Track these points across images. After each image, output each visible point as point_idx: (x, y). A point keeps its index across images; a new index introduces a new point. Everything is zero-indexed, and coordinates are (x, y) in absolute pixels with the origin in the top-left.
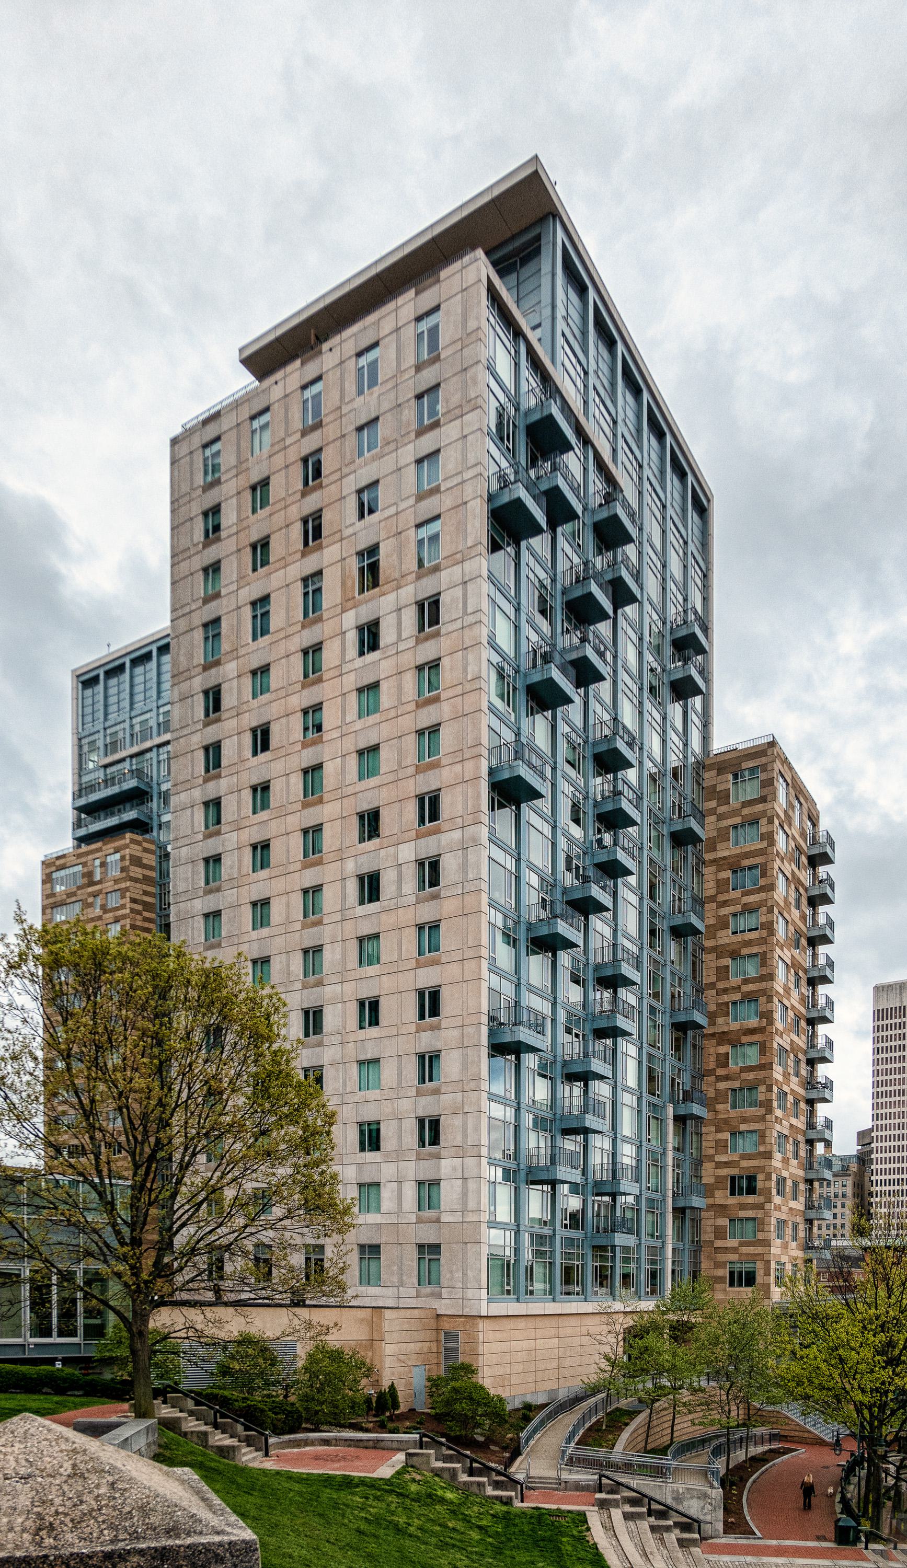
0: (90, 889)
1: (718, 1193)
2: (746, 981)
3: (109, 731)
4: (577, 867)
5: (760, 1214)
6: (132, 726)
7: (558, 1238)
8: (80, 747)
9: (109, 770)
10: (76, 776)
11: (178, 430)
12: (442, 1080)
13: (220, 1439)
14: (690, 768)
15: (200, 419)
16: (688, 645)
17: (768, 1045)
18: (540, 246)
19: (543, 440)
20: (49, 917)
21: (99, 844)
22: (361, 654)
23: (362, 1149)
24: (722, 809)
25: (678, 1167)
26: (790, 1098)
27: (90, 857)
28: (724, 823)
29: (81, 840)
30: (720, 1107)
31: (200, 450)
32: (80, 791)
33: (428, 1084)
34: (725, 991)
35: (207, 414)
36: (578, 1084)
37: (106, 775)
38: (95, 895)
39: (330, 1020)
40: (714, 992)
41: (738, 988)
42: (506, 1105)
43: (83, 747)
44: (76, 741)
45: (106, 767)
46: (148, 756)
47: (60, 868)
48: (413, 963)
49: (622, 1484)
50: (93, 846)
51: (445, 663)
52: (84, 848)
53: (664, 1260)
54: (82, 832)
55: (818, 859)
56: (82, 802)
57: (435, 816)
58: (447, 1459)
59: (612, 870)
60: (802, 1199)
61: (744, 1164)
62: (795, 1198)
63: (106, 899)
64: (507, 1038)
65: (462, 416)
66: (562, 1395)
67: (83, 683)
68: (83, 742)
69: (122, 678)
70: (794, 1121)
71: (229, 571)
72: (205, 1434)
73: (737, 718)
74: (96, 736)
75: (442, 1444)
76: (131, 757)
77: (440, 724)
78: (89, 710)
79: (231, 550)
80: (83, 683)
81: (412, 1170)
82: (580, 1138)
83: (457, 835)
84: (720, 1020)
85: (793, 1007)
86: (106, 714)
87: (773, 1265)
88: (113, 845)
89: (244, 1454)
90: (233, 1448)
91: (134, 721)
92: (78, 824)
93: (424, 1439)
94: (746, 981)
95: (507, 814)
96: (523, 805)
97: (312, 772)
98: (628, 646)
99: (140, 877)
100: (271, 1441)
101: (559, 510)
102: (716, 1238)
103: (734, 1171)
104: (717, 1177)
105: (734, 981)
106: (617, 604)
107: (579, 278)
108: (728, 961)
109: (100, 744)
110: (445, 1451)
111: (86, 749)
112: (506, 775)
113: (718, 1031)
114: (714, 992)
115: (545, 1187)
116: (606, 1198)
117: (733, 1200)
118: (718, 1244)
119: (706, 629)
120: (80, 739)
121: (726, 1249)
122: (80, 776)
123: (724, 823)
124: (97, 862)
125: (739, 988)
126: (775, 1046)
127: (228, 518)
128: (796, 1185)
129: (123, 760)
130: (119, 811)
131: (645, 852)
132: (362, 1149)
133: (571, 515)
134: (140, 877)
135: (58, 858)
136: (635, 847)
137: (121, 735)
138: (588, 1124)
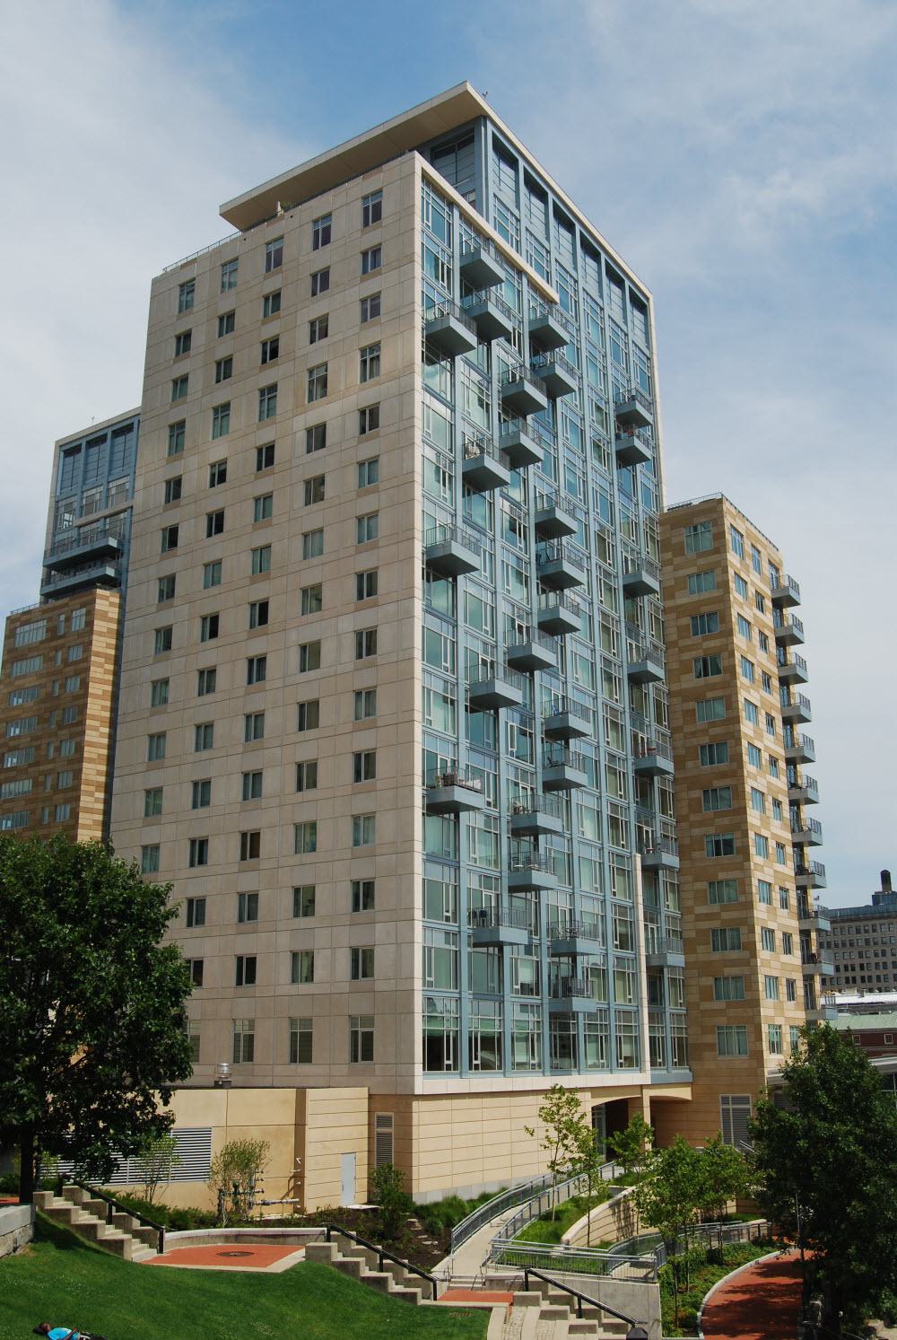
0: (53, 644)
1: (701, 949)
2: (713, 724)
3: (85, 495)
4: (520, 627)
5: (746, 971)
6: (108, 490)
7: (612, 1011)
8: (57, 509)
9: (82, 530)
10: (51, 536)
11: (159, 272)
12: (377, 842)
13: (110, 1232)
14: (642, 527)
15: (179, 264)
16: (629, 420)
17: (740, 789)
18: (473, 137)
19: (475, 278)
20: (8, 671)
21: (65, 600)
22: (309, 451)
23: (296, 915)
24: (677, 560)
25: (652, 921)
26: (772, 843)
27: (56, 612)
28: (681, 573)
29: (47, 596)
30: (696, 854)
31: (177, 290)
32: (53, 549)
33: (363, 847)
34: (693, 734)
35: (185, 261)
36: (527, 838)
37: (79, 534)
38: (56, 649)
39: (269, 783)
40: (682, 735)
41: (704, 732)
42: (444, 864)
43: (59, 507)
44: (53, 503)
45: (80, 527)
46: (122, 516)
47: (23, 624)
48: (349, 727)
49: (550, 1281)
50: (61, 602)
51: (383, 460)
52: (52, 603)
53: (639, 1027)
54: (51, 588)
55: (783, 601)
56: (54, 560)
57: (372, 591)
58: (408, 1282)
59: (554, 627)
60: (797, 953)
61: (725, 915)
62: (788, 951)
63: (68, 653)
64: (443, 798)
65: (400, 267)
66: (512, 1187)
67: (65, 451)
68: (60, 504)
69: (102, 446)
70: (779, 867)
71: (194, 386)
72: (94, 1227)
73: (681, 481)
74: (73, 499)
75: (351, 1237)
76: (105, 518)
77: (378, 511)
78: (68, 476)
79: (198, 367)
80: (65, 451)
81: (349, 937)
82: (531, 895)
83: (392, 608)
84: (690, 764)
85: (767, 748)
86: (85, 479)
87: (765, 1028)
88: (78, 601)
89: (137, 1250)
90: (121, 1242)
91: (111, 485)
92: (47, 580)
93: (332, 1233)
94: (713, 724)
95: (441, 585)
96: (460, 578)
97: (262, 552)
98: (584, 410)
99: (105, 630)
100: (167, 1236)
101: (488, 330)
102: (702, 999)
103: (716, 924)
104: (698, 931)
105: (701, 724)
106: (552, 397)
107: (507, 155)
108: (692, 705)
109: (76, 505)
110: (354, 1246)
111: (62, 510)
112: (440, 553)
113: (695, 778)
114: (682, 735)
115: (491, 949)
116: (564, 959)
117: (717, 956)
118: (705, 1006)
119: (651, 405)
120: (57, 502)
121: (714, 1012)
122: (54, 535)
123: (681, 573)
124: (62, 617)
125: (707, 731)
126: (748, 789)
127: (197, 341)
128: (787, 937)
129: (98, 520)
130: (90, 567)
131: (596, 607)
132: (296, 915)
133: (501, 331)
134: (105, 630)
135: (24, 613)
136: (585, 603)
137: (98, 497)
138: (535, 882)
